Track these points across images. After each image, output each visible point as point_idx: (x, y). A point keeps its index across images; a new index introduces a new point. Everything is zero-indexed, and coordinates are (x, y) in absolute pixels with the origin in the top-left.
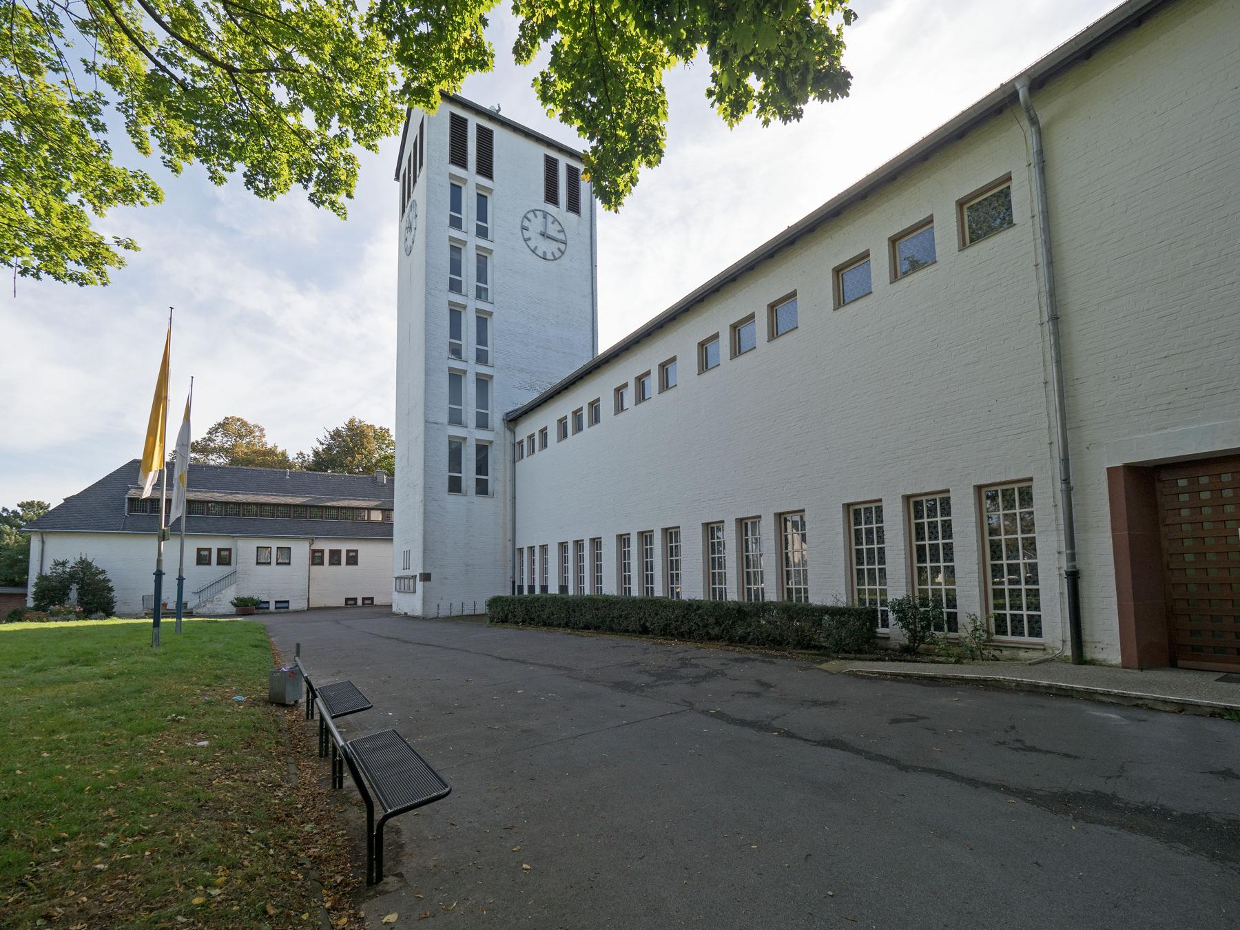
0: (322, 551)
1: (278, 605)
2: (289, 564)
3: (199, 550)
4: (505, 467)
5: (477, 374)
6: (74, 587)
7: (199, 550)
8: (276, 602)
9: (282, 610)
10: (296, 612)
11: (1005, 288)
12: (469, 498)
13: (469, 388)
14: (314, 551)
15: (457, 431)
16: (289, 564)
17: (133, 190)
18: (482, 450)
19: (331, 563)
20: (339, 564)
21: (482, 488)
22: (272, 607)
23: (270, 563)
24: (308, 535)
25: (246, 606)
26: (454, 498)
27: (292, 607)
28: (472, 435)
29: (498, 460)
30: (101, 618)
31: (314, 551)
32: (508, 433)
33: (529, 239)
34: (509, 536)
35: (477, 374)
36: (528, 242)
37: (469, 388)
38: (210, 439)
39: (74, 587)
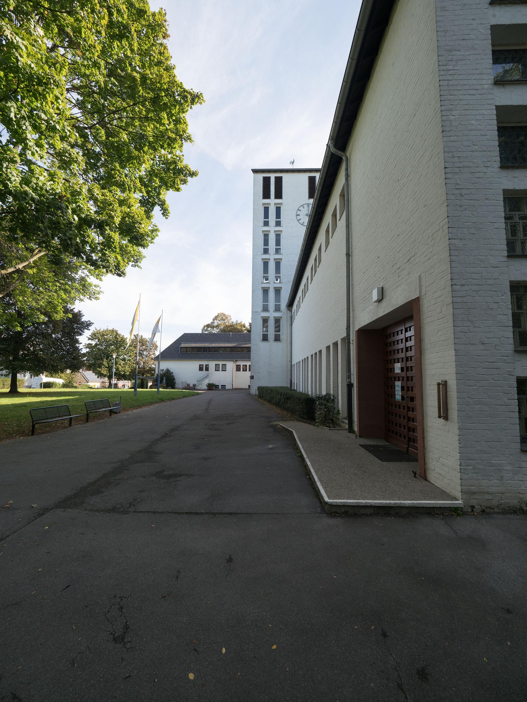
0: (240, 365)
1: (222, 387)
2: (226, 371)
3: (200, 365)
4: (287, 327)
5: (274, 288)
6: (165, 378)
7: (200, 365)
8: (222, 386)
9: (224, 389)
10: (228, 390)
11: (457, 170)
12: (271, 344)
13: (272, 294)
14: (237, 366)
15: (265, 314)
16: (226, 371)
17: (8, 293)
18: (277, 321)
19: (243, 370)
20: (240, 371)
21: (277, 339)
22: (220, 387)
23: (219, 370)
24: (234, 359)
25: (211, 387)
26: (265, 343)
27: (227, 388)
28: (272, 314)
29: (284, 324)
30: (170, 389)
31: (237, 366)
32: (289, 312)
33: (300, 219)
34: (289, 359)
35: (274, 288)
36: (300, 221)
37: (272, 294)
38: (213, 323)
39: (165, 378)
